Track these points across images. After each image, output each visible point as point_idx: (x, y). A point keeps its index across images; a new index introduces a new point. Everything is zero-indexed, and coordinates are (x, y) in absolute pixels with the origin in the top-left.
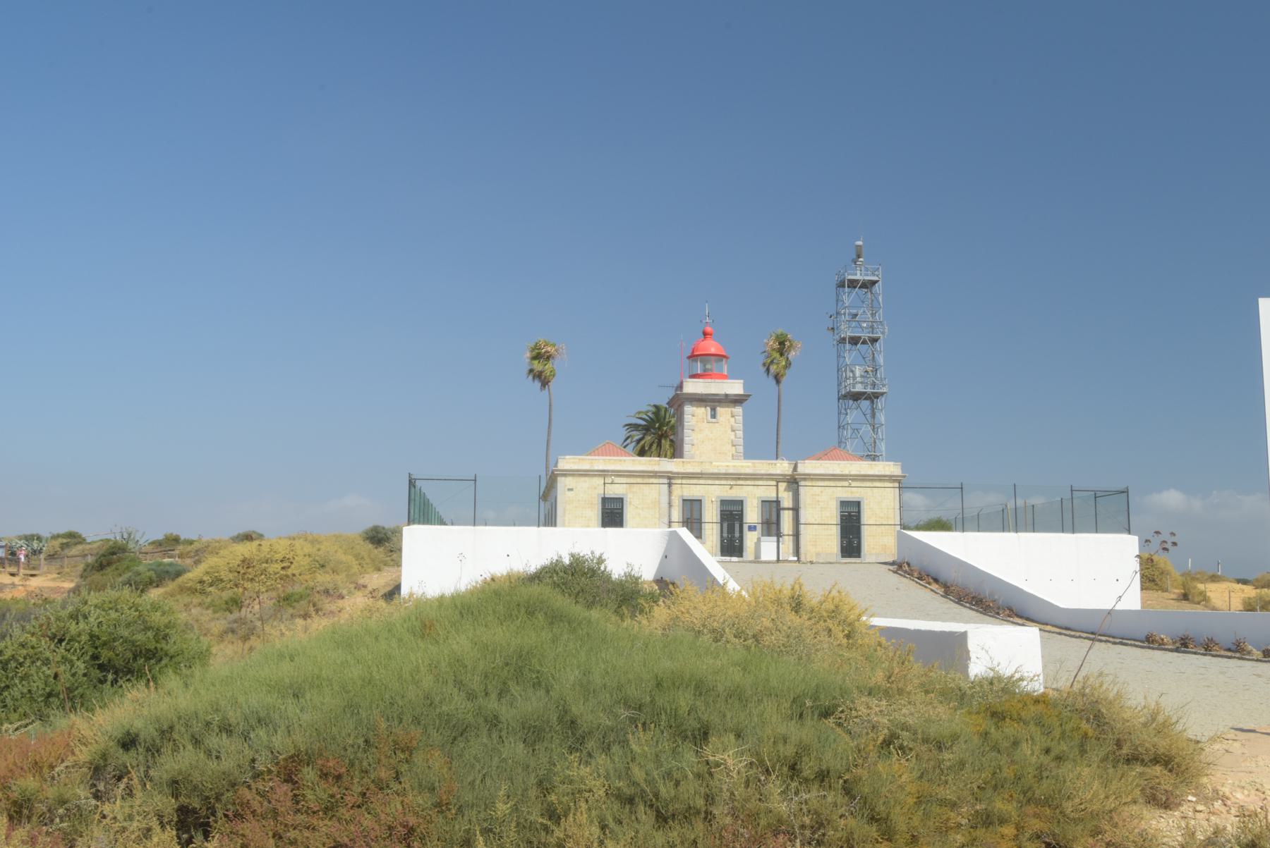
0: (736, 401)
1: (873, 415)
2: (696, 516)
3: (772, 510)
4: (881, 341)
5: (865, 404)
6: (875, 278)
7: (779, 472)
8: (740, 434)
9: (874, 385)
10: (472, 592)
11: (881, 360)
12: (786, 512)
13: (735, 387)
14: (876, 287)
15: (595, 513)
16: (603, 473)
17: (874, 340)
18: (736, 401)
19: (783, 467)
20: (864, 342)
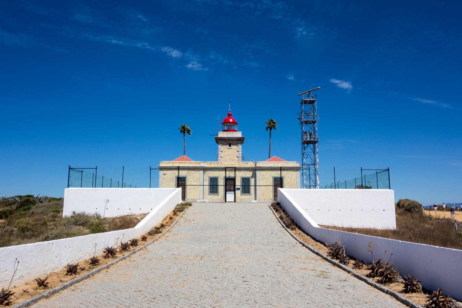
0: (239, 141)
1: (315, 149)
2: (215, 184)
3: (246, 181)
4: (317, 122)
5: (311, 145)
6: (314, 99)
7: (249, 166)
8: (240, 153)
9: (315, 138)
10: (304, 218)
11: (317, 129)
12: (180, 173)
13: (238, 135)
14: (316, 103)
15: (174, 182)
16: (178, 168)
17: (314, 122)
18: (239, 141)
19: (251, 164)
20: (310, 123)
